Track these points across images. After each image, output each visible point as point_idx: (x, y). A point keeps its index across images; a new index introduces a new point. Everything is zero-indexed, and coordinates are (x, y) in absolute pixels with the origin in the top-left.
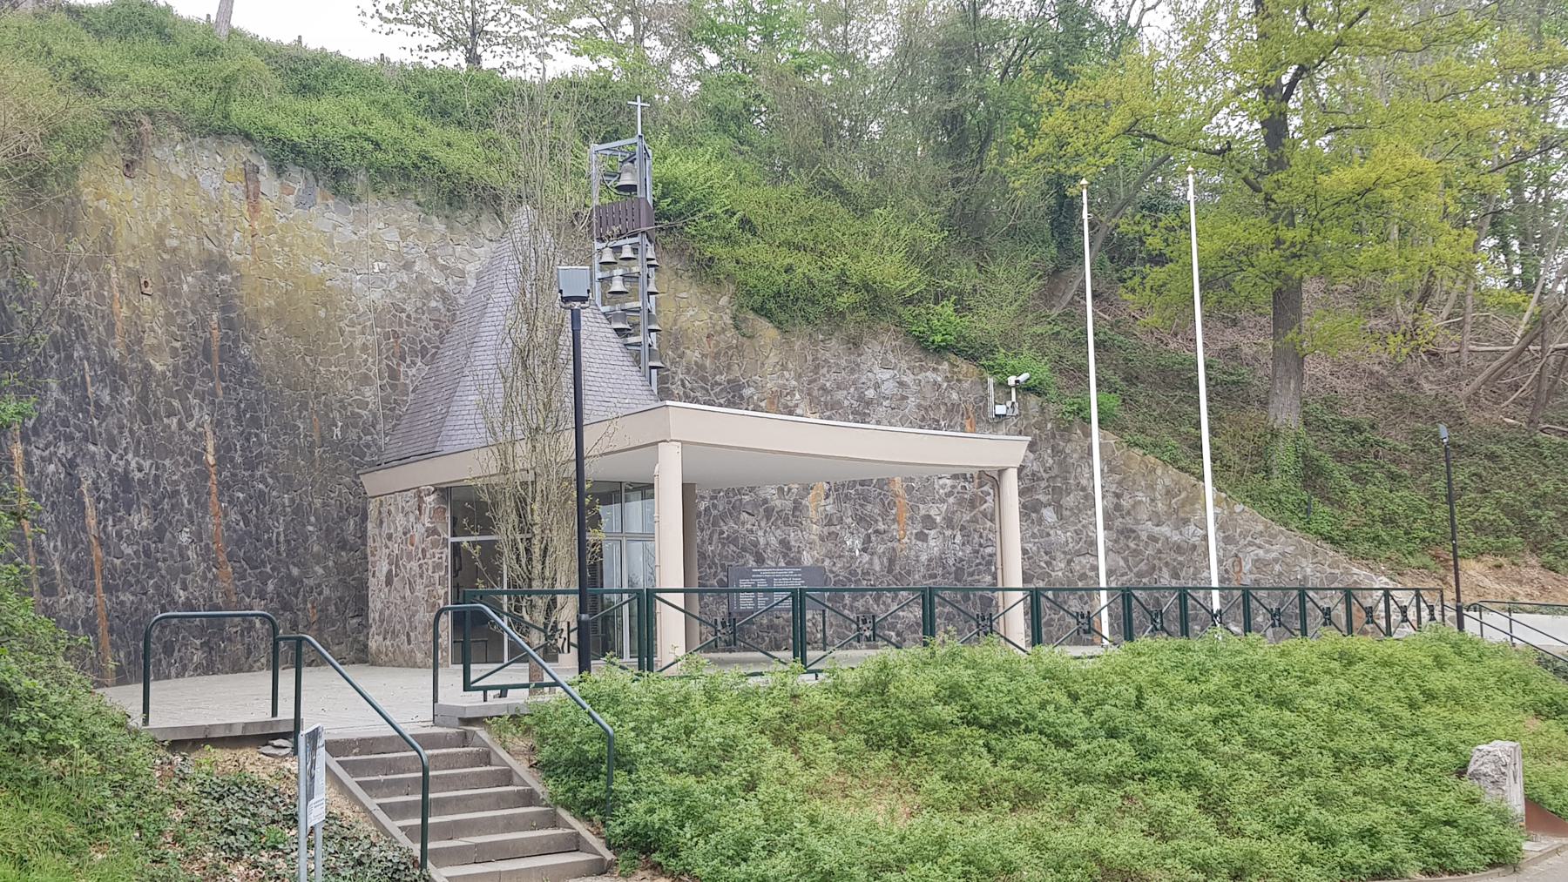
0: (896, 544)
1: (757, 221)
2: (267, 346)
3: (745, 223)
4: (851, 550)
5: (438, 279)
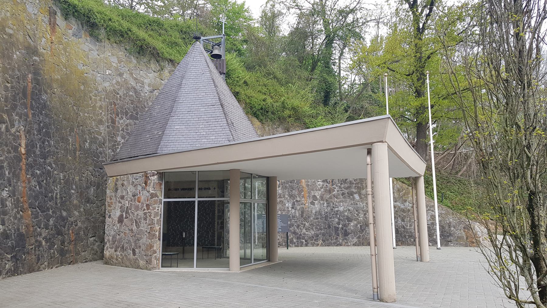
0: (303, 206)
1: (249, 83)
2: (55, 97)
3: (245, 82)
4: (288, 208)
5: (133, 83)
